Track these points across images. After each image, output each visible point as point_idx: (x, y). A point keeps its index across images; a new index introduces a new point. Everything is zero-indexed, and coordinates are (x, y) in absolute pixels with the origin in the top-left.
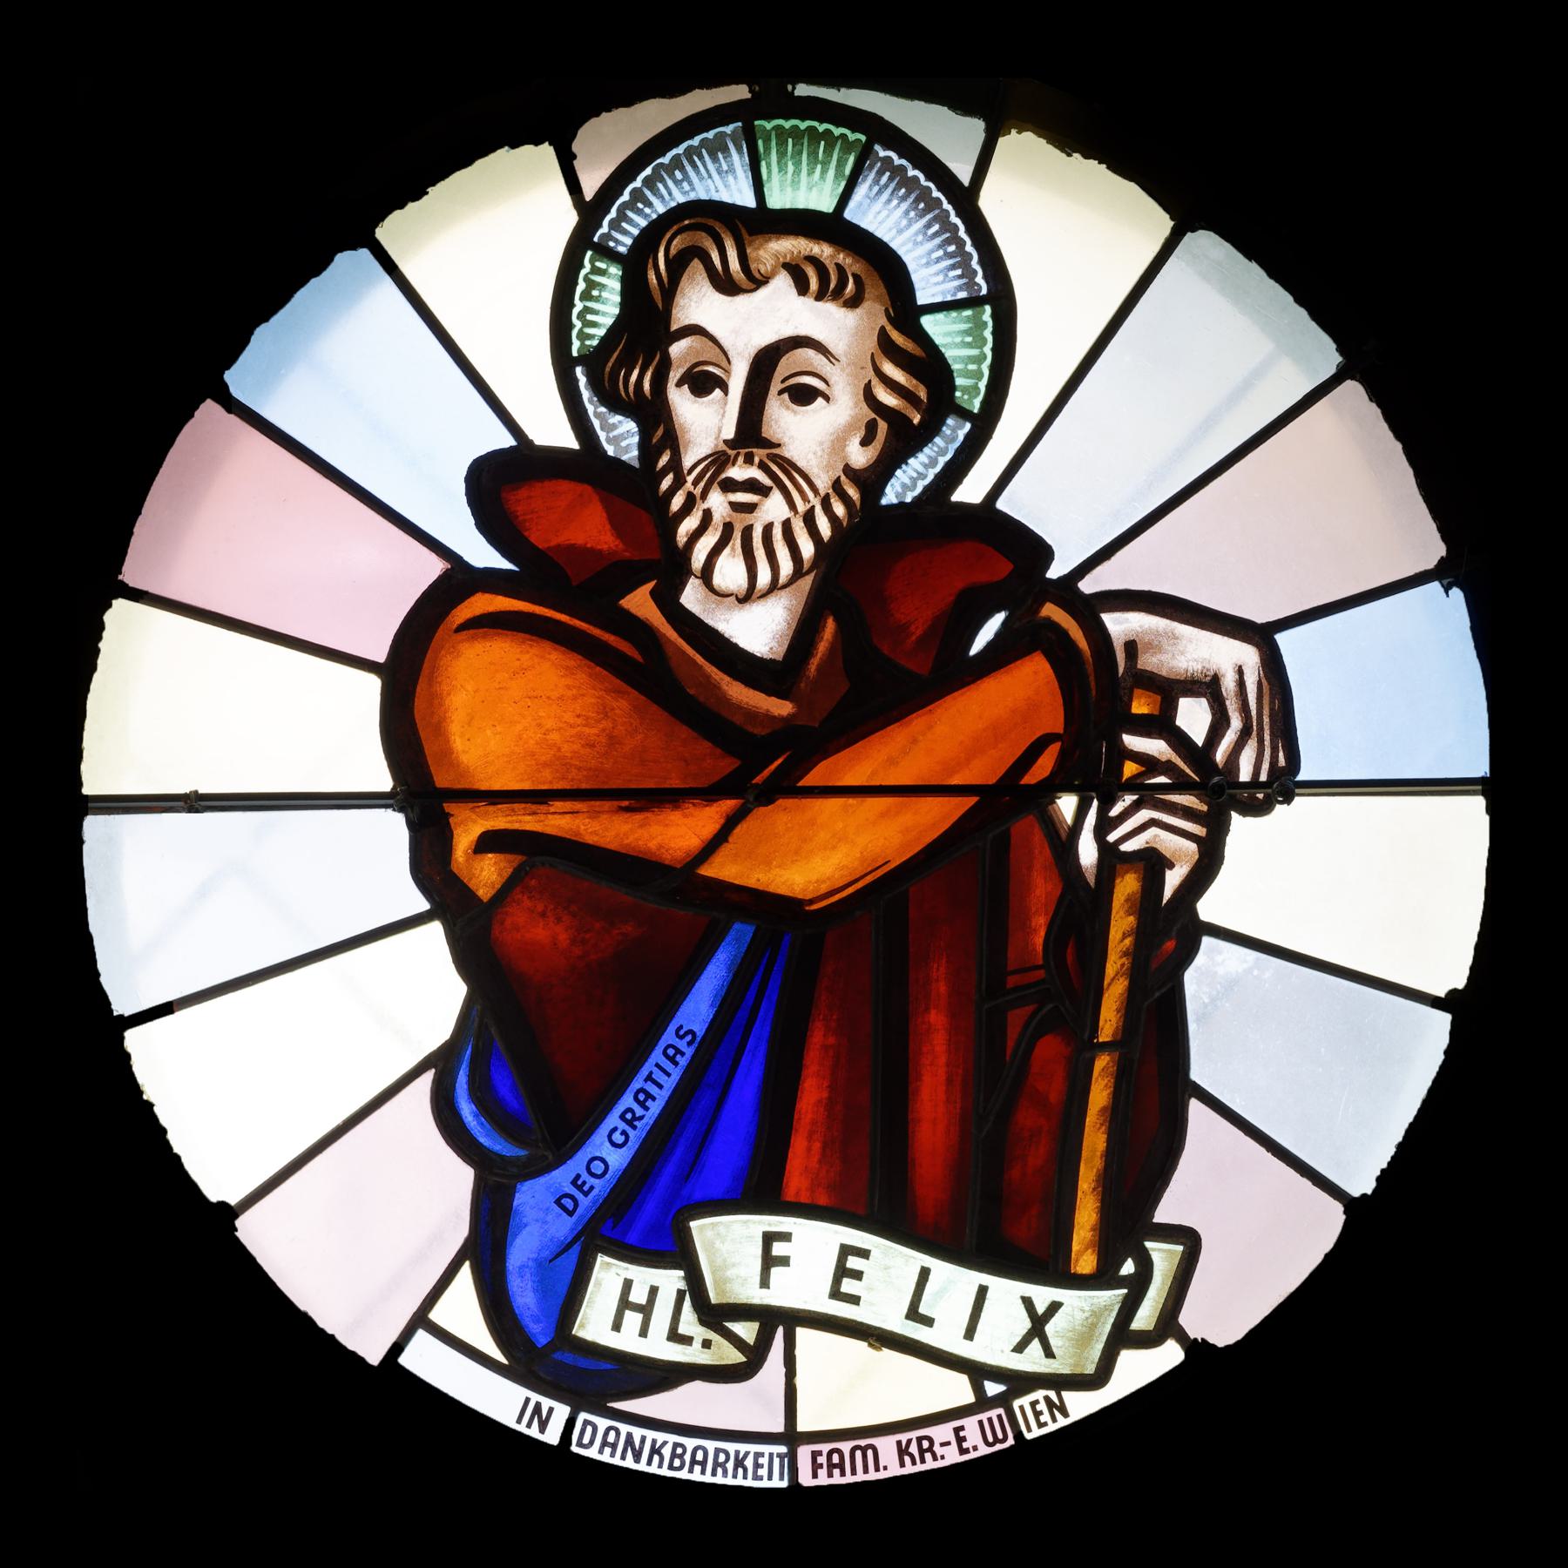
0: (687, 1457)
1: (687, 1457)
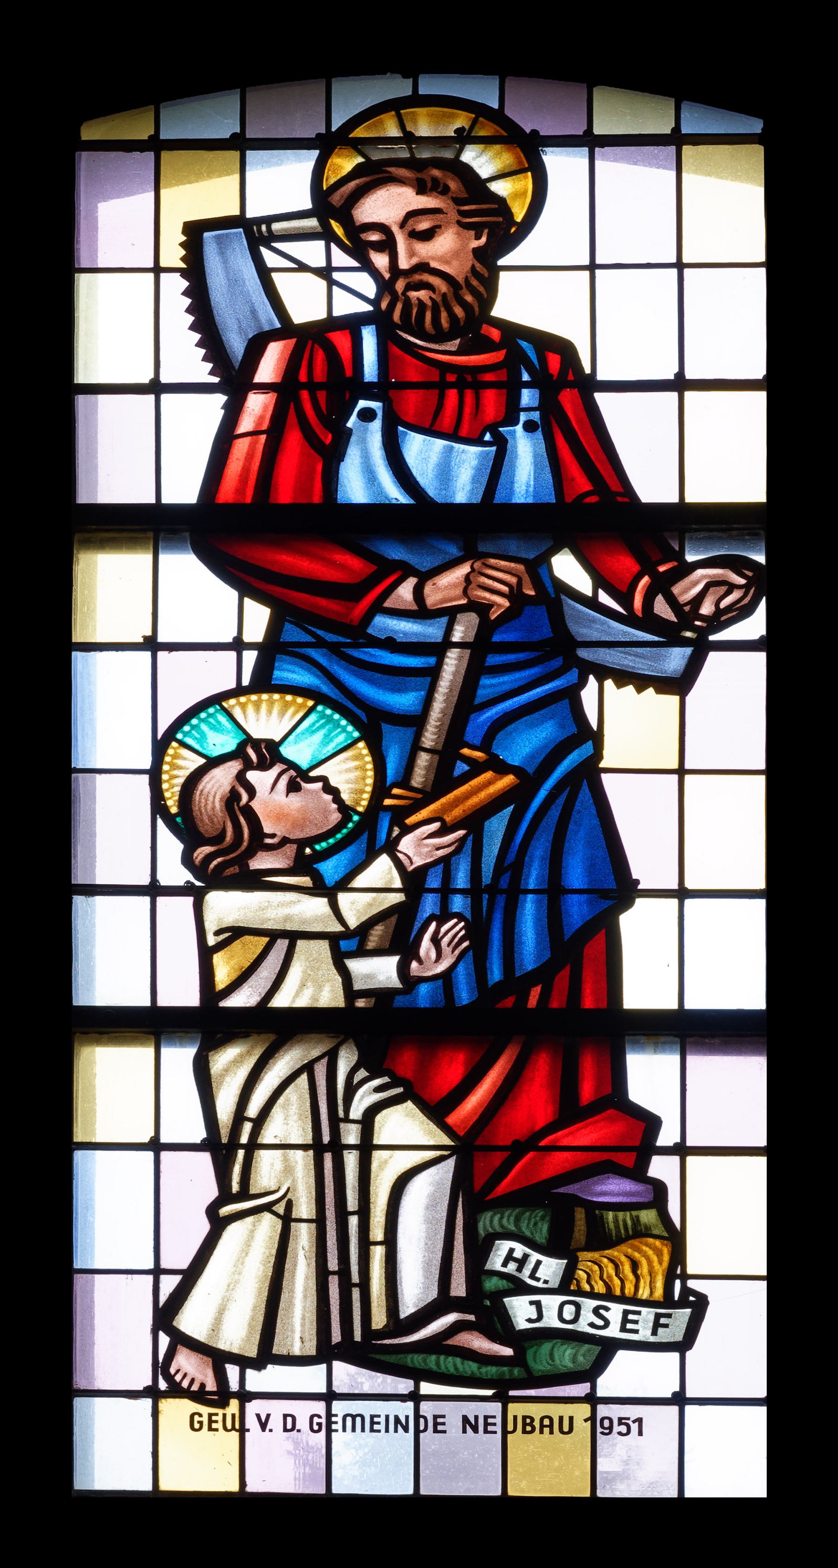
0: (537, 1424)
1: (537, 1424)
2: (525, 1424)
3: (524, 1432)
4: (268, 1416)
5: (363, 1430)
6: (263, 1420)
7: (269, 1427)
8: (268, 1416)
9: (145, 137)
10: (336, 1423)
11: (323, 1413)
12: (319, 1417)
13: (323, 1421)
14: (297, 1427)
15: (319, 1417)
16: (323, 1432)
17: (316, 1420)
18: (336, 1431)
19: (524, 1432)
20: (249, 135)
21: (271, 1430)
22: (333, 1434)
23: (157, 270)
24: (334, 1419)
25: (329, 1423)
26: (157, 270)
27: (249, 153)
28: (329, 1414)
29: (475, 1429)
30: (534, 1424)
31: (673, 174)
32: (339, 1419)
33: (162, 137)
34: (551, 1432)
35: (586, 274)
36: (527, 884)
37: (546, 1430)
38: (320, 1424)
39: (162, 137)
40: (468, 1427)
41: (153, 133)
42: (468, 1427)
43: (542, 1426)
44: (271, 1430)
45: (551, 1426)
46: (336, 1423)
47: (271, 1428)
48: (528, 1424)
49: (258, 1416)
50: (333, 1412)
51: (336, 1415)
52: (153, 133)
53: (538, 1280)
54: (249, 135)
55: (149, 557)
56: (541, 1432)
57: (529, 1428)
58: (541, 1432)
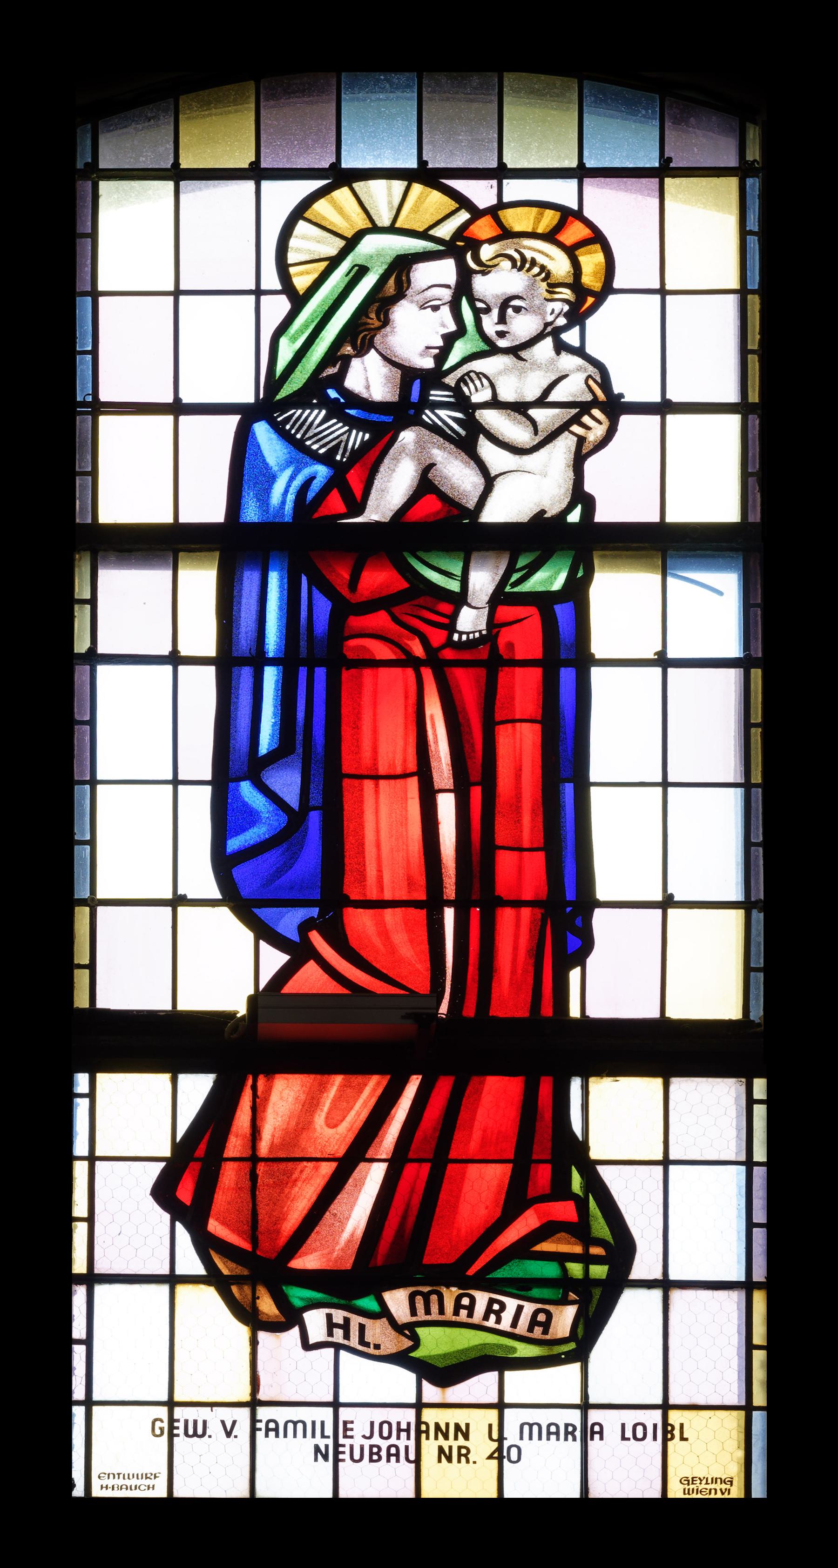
0: (384, 1453)
1: (384, 1453)
2: (371, 1454)
3: (371, 1460)
4: (234, 1422)
5: (540, 1438)
6: (229, 1429)
7: (234, 1434)
8: (234, 1422)
9: (326, 165)
10: (343, 1453)
11: (166, 1419)
12: (162, 1421)
13: (165, 1425)
14: (208, 1432)
15: (162, 1421)
16: (166, 1436)
17: (158, 1424)
18: (343, 1460)
19: (371, 1460)
20: (263, 165)
21: (236, 1437)
22: (175, 1439)
23: (258, 292)
24: (341, 1449)
25: (171, 1427)
26: (258, 292)
27: (505, 182)
28: (172, 1420)
29: (449, 1459)
30: (381, 1453)
31: (656, 202)
32: (181, 1425)
33: (344, 166)
34: (398, 1461)
35: (171, 299)
36: (533, 915)
37: (393, 1459)
38: (162, 1429)
39: (344, 166)
40: (443, 1456)
41: (254, 159)
42: (443, 1457)
43: (389, 1455)
44: (236, 1437)
45: (397, 1455)
46: (343, 1453)
47: (210, 1434)
48: (375, 1454)
49: (223, 1422)
50: (176, 1417)
51: (344, 1446)
52: (254, 159)
53: (367, 1345)
54: (263, 165)
55: (169, 573)
56: (388, 1460)
57: (375, 1457)
58: (388, 1460)
